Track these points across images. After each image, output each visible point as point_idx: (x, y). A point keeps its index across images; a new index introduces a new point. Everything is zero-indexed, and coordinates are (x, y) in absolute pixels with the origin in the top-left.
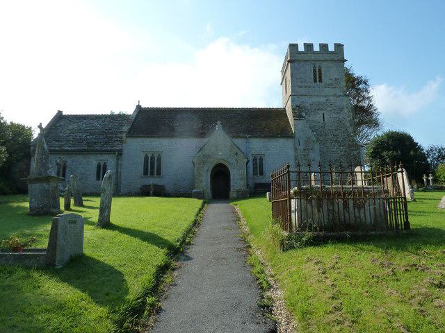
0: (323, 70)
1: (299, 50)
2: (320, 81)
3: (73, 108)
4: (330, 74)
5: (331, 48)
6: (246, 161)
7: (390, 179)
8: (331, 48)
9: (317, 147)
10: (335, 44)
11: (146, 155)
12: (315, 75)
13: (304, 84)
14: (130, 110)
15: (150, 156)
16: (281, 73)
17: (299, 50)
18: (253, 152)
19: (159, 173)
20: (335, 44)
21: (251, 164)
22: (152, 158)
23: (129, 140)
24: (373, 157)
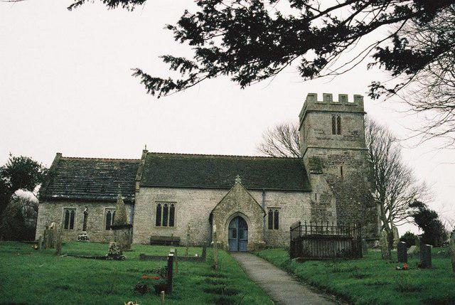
0: (343, 121)
1: (349, 101)
2: (339, 133)
3: (72, 151)
4: (348, 124)
5: (351, 100)
6: (263, 214)
7: (380, 206)
8: (351, 100)
9: (333, 202)
10: (339, 95)
11: (159, 205)
12: (334, 126)
13: (322, 136)
14: (138, 155)
15: (162, 206)
16: (299, 119)
17: (349, 101)
18: (268, 205)
19: (172, 224)
20: (339, 95)
21: (267, 217)
22: (166, 209)
23: (142, 190)
24: (225, 42)
